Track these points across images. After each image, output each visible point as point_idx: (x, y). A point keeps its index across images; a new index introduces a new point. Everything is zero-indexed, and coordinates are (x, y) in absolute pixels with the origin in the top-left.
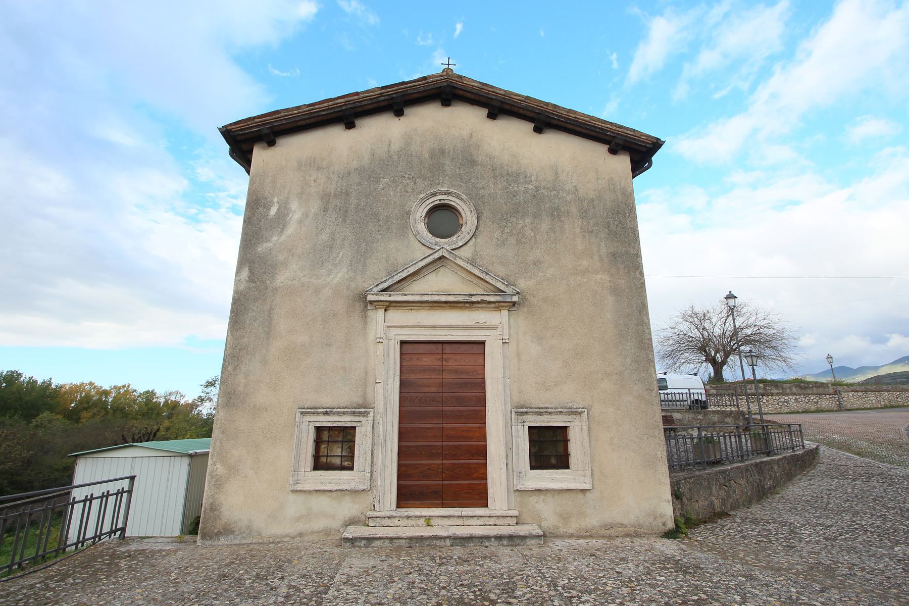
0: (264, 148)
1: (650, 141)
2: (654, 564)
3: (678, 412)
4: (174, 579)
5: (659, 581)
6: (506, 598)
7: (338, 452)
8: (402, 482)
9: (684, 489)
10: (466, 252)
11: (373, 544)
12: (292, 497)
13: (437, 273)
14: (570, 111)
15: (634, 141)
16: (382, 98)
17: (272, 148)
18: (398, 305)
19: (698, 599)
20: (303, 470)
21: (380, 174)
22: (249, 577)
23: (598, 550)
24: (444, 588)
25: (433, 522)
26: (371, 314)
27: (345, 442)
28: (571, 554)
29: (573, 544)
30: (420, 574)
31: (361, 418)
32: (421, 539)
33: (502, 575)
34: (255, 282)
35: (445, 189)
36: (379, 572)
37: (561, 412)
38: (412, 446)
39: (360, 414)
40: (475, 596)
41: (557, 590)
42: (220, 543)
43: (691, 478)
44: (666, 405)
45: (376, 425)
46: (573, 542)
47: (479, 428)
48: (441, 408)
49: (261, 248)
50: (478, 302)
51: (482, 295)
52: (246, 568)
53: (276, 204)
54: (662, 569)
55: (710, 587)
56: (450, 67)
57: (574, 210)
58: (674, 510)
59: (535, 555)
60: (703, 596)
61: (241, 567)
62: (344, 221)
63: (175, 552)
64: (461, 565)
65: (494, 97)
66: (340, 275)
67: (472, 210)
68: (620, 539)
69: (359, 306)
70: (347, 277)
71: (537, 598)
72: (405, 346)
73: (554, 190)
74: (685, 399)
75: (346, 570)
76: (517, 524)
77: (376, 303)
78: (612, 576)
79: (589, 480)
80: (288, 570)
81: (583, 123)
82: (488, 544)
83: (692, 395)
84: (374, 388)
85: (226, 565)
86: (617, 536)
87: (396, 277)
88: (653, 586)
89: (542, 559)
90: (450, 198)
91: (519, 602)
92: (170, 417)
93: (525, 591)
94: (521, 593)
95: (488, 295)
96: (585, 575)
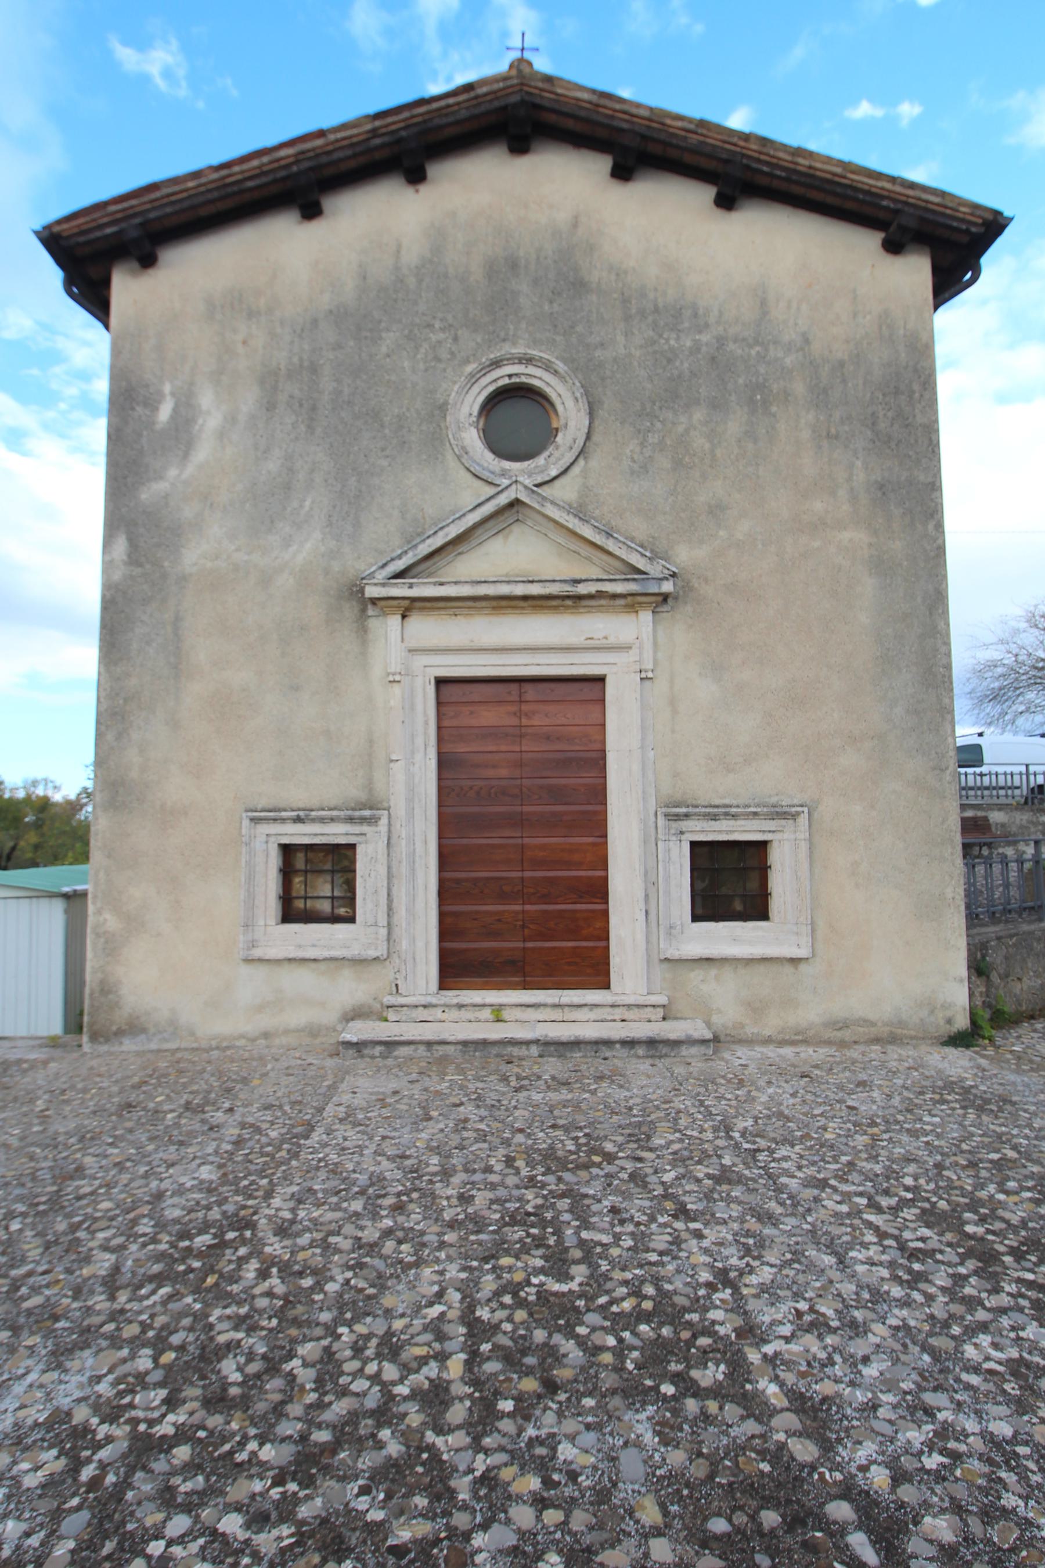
0: (134, 274)
1: (979, 217)
2: (922, 1093)
3: (1000, 810)
4: (42, 1111)
5: (928, 1124)
6: (633, 1150)
7: (326, 890)
8: (448, 945)
9: (995, 957)
10: (566, 490)
11: (396, 1053)
12: (245, 970)
13: (506, 537)
14: (800, 152)
15: (942, 220)
16: (377, 141)
17: (151, 271)
18: (428, 604)
19: (1001, 1159)
20: (262, 923)
21: (380, 321)
22: (172, 1107)
23: (816, 1067)
24: (521, 1131)
25: (506, 1014)
26: (374, 624)
27: (338, 871)
28: (764, 1073)
29: (770, 1054)
30: (478, 1107)
31: (365, 828)
32: (484, 1043)
33: (630, 1109)
34: (141, 565)
35: (519, 350)
36: (405, 1100)
37: (755, 814)
38: (467, 880)
39: (363, 820)
40: (579, 1146)
41: (731, 1138)
42: (124, 1048)
43: (1011, 936)
44: (976, 796)
45: (393, 841)
46: (771, 1052)
47: (594, 844)
48: (518, 809)
49: (149, 493)
50: (590, 597)
51: (598, 580)
52: (167, 1091)
53: (168, 397)
54: (935, 1102)
55: (1027, 1137)
56: (527, 55)
57: (799, 388)
58: (971, 995)
59: (695, 1074)
60: (1011, 1154)
61: (160, 1090)
62: (311, 429)
63: (45, 1063)
64: (555, 1090)
65: (625, 126)
66: (308, 546)
67: (578, 395)
68: (861, 1048)
69: (350, 610)
70: (323, 549)
71: (691, 1151)
72: (446, 689)
73: (757, 342)
74: (1017, 783)
75: (346, 1098)
76: (664, 1019)
77: (383, 603)
78: (838, 1114)
79: (806, 940)
80: (242, 1096)
81: (828, 181)
82: (608, 1054)
83: (1032, 777)
84: (388, 770)
85: (133, 1087)
86: (855, 1042)
87: (421, 547)
88: (914, 1134)
89: (709, 1081)
90: (531, 370)
91: (658, 1157)
92: (38, 825)
93: (671, 1137)
94: (662, 1142)
95: (610, 580)
96: (786, 1112)
